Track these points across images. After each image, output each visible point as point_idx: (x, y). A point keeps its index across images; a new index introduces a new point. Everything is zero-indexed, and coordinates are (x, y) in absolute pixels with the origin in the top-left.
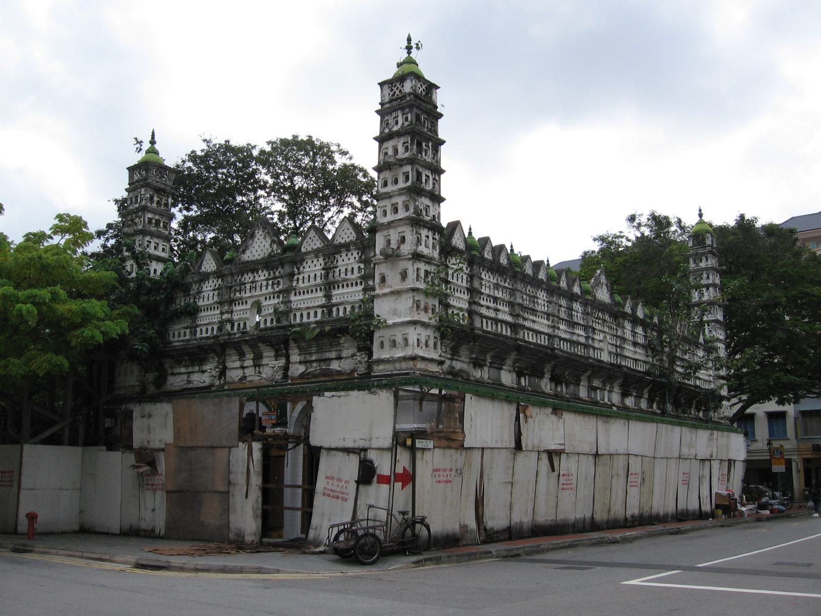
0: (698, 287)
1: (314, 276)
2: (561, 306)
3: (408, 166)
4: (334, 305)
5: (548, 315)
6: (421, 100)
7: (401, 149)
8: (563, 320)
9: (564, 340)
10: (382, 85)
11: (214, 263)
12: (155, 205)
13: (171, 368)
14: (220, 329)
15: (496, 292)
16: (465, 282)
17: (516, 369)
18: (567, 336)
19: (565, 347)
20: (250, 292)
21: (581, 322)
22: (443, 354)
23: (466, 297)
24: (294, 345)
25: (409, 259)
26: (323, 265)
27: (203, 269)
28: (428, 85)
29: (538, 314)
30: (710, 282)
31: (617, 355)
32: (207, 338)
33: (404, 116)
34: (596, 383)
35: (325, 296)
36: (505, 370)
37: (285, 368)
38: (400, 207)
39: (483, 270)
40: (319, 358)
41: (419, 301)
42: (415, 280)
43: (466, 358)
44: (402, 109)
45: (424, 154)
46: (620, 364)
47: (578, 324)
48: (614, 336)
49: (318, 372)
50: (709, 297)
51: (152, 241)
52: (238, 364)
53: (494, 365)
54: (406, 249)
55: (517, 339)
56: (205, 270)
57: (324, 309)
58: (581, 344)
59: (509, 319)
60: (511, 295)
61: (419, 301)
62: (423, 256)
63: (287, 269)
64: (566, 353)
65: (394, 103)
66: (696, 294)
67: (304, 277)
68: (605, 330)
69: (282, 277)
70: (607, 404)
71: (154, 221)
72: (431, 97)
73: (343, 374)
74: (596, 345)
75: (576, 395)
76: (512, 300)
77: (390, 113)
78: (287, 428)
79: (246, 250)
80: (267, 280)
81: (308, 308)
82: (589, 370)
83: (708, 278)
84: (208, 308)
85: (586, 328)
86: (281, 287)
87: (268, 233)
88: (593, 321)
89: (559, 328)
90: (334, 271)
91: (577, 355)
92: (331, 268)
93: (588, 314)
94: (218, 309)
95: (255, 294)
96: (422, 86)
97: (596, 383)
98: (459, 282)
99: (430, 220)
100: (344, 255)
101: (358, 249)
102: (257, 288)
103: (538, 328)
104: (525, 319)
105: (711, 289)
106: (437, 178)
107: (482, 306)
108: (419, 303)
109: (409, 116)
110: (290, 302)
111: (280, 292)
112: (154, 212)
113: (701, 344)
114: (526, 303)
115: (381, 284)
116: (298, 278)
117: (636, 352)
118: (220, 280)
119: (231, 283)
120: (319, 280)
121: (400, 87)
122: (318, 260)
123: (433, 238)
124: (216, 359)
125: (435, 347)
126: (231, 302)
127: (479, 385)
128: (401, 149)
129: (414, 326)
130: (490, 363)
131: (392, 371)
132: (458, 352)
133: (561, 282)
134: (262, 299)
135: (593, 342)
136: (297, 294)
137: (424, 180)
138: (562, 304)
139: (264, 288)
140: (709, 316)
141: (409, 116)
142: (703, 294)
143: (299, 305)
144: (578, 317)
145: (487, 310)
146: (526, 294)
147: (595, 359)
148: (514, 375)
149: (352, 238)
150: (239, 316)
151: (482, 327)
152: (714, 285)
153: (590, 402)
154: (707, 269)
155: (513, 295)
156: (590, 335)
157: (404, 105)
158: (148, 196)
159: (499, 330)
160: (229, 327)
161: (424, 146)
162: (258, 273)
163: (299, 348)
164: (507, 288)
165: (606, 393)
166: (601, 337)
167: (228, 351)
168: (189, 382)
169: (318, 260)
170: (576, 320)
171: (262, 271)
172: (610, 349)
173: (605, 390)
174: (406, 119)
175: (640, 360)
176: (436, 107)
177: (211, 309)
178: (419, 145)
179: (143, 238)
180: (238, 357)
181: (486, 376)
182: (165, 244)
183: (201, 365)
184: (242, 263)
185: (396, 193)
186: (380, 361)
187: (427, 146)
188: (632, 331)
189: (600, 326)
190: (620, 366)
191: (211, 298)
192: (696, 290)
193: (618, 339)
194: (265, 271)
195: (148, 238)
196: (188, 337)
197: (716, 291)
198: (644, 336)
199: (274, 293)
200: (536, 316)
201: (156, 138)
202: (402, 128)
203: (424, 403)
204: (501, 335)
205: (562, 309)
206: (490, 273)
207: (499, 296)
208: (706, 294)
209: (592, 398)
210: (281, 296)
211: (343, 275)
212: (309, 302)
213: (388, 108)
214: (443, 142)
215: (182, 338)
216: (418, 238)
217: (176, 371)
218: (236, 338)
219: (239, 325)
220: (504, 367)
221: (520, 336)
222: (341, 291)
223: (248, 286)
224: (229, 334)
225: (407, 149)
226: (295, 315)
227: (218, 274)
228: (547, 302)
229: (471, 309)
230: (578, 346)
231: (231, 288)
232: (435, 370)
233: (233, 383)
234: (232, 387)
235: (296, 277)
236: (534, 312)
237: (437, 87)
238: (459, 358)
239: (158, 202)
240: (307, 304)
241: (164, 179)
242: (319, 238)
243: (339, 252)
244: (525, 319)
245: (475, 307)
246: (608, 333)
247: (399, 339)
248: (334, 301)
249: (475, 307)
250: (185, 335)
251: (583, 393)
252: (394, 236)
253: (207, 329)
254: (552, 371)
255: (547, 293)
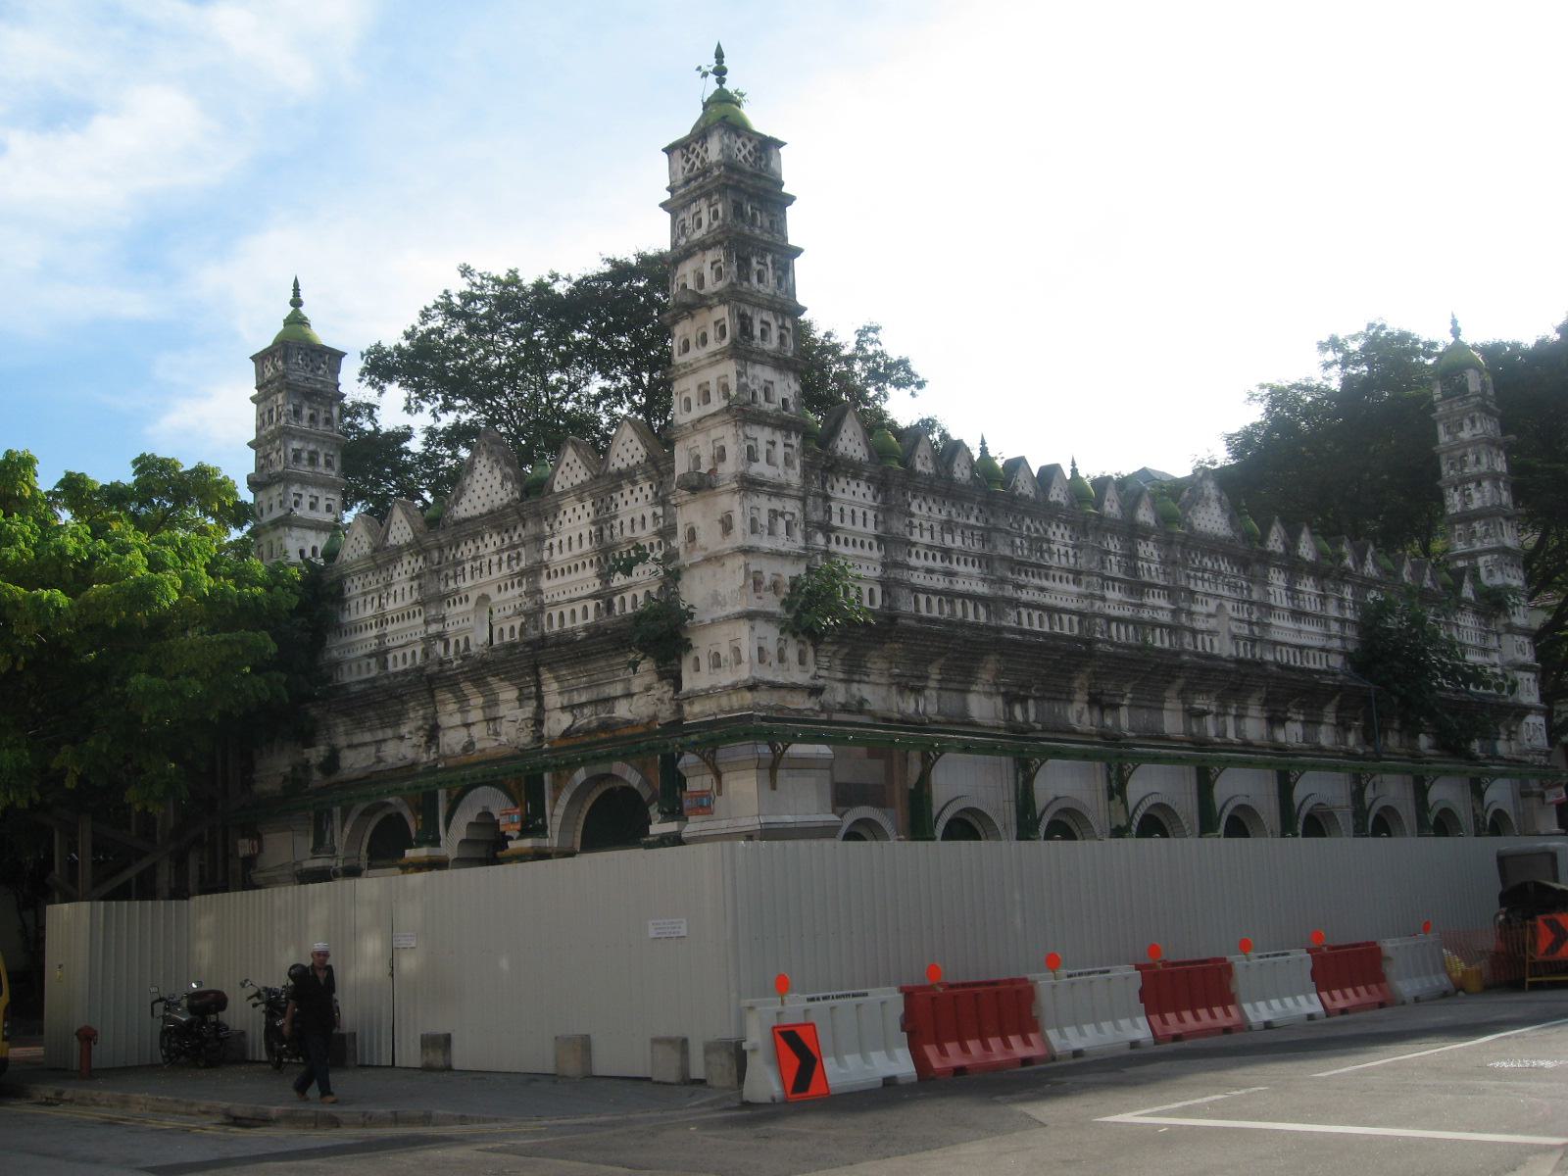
0: (1461, 483)
2: (1108, 552)
5: (1077, 575)
8: (1114, 579)
9: (1119, 620)
10: (669, 150)
12: (305, 424)
13: (347, 734)
15: (948, 538)
17: (1002, 690)
20: (472, 577)
21: (1161, 581)
23: (876, 554)
24: (548, 675)
26: (592, 515)
27: (392, 541)
30: (1483, 468)
34: (1200, 703)
36: (978, 692)
40: (594, 697)
42: (748, 531)
44: (708, 195)
47: (1154, 586)
48: (1244, 602)
49: (595, 724)
50: (1484, 502)
51: (303, 492)
52: (457, 719)
54: (729, 468)
55: (999, 630)
57: (599, 601)
58: (1162, 626)
59: (981, 589)
62: (762, 484)
63: (531, 528)
64: (1123, 648)
65: (693, 184)
66: (1457, 496)
68: (1220, 592)
69: (523, 544)
70: (1231, 744)
71: (305, 455)
72: (767, 165)
76: (986, 550)
77: (685, 207)
78: (546, 837)
79: (460, 498)
80: (499, 551)
81: (572, 601)
83: (1478, 461)
85: (1171, 592)
87: (497, 461)
89: (1103, 599)
90: (612, 526)
92: (606, 521)
93: (1174, 563)
94: (420, 614)
95: (481, 581)
96: (744, 145)
97: (1200, 703)
99: (776, 410)
101: (649, 478)
104: (1019, 587)
105: (1486, 484)
107: (916, 569)
108: (759, 577)
109: (720, 207)
110: (540, 592)
111: (522, 573)
112: (304, 436)
113: (1467, 601)
114: (1023, 553)
115: (689, 545)
116: (551, 544)
117: (1300, 631)
120: (586, 546)
122: (583, 507)
125: (802, 662)
126: (442, 598)
131: (715, 714)
132: (860, 666)
133: (1106, 503)
134: (492, 591)
137: (757, 332)
139: (495, 568)
140: (1486, 541)
141: (720, 207)
142: (1469, 495)
143: (556, 596)
145: (928, 576)
146: (1021, 536)
148: (999, 701)
150: (456, 627)
152: (1495, 477)
154: (1474, 442)
155: (989, 541)
156: (1184, 605)
157: (710, 187)
158: (291, 407)
159: (959, 614)
160: (439, 647)
162: (482, 539)
164: (973, 527)
165: (1230, 722)
167: (440, 696)
168: (380, 760)
169: (583, 507)
172: (1235, 630)
173: (1226, 714)
174: (716, 215)
175: (1310, 648)
178: (744, 264)
179: (286, 488)
180: (457, 706)
182: (331, 496)
183: (397, 724)
185: (703, 362)
186: (694, 696)
188: (1287, 589)
189: (1207, 584)
192: (1456, 490)
193: (1255, 608)
194: (495, 536)
195: (295, 489)
196: (373, 674)
197: (1497, 487)
198: (1319, 596)
200: (1047, 579)
201: (301, 293)
202: (708, 233)
203: (780, 773)
205: (1112, 557)
208: (1476, 495)
209: (1192, 735)
210: (524, 581)
211: (627, 533)
212: (573, 590)
213: (683, 196)
214: (797, 252)
215: (365, 676)
216: (749, 448)
217: (356, 740)
219: (457, 642)
220: (974, 688)
223: (468, 567)
224: (441, 663)
225: (719, 274)
226: (550, 616)
232: (802, 707)
233: (454, 756)
234: (451, 762)
235: (547, 543)
237: (782, 144)
238: (866, 678)
239: (312, 418)
240: (572, 595)
241: (320, 372)
244: (1019, 587)
246: (1228, 599)
247: (725, 652)
250: (369, 670)
251: (1172, 722)
255: (1073, 529)
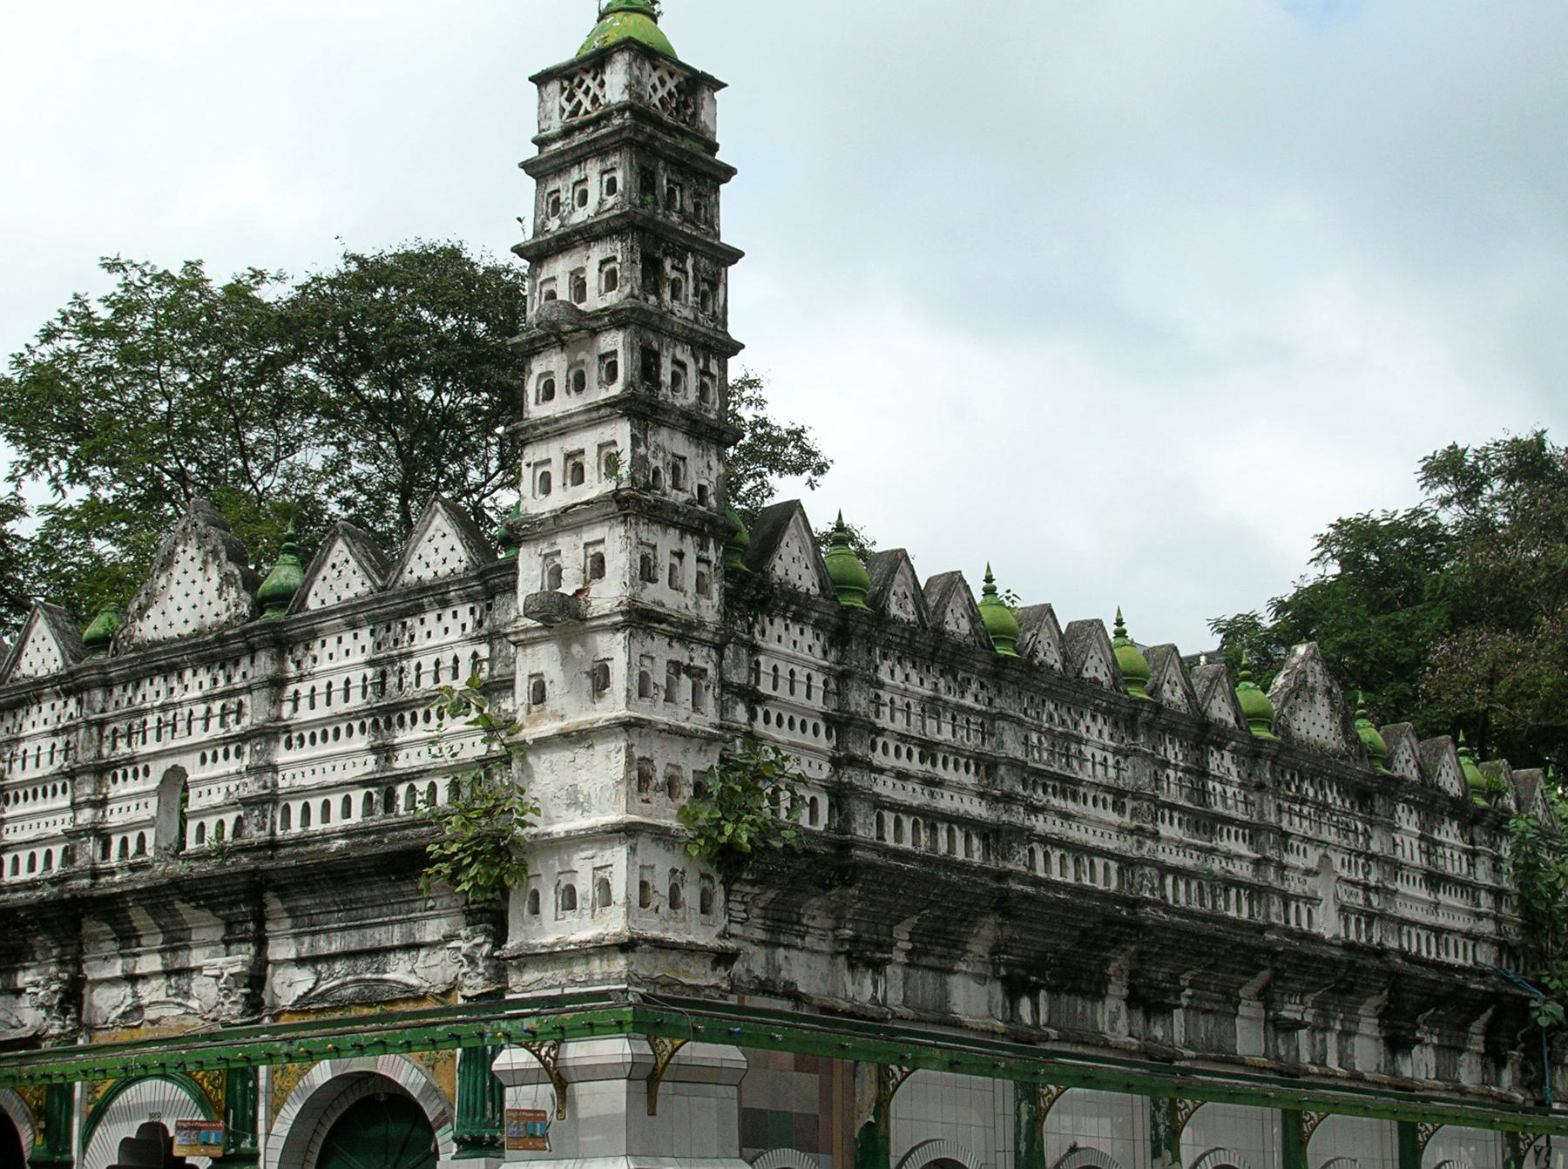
1: (450, 663)
2: (1165, 764)
3: (613, 333)
4: (399, 779)
5: (1118, 797)
6: (657, 122)
7: (593, 278)
8: (1173, 807)
9: (1178, 872)
11: (56, 651)
14: (68, 857)
15: (931, 724)
16: (818, 694)
17: (1003, 972)
18: (1188, 861)
19: (1179, 894)
20: (159, 739)
21: (1238, 813)
22: (736, 929)
23: (823, 743)
25: (615, 628)
28: (687, 80)
29: (1082, 790)
31: (1371, 917)
32: (31, 885)
33: (606, 177)
35: (373, 750)
37: (251, 977)
38: (590, 461)
39: (885, 656)
41: (650, 761)
42: (635, 695)
43: (823, 938)
45: (667, 296)
46: (1380, 944)
47: (1230, 821)
53: (924, 961)
54: (607, 596)
56: (30, 672)
57: (371, 790)
58: (1239, 884)
59: (977, 809)
60: (985, 734)
61: (650, 761)
62: (661, 619)
63: (264, 666)
64: (1181, 916)
65: (578, 138)
67: (313, 689)
68: (1325, 836)
69: (249, 690)
72: (695, 115)
73: (421, 998)
74: (1294, 886)
75: (1220, 1050)
76: (987, 748)
77: (560, 171)
79: (147, 607)
80: (206, 699)
82: (1263, 968)
84: (35, 792)
85: (1254, 831)
86: (246, 721)
87: (215, 553)
88: (1280, 809)
89: (1156, 836)
90: (402, 670)
91: (1223, 920)
92: (391, 660)
93: (1260, 787)
94: (64, 792)
96: (663, 83)
98: (800, 697)
99: (688, 502)
100: (430, 617)
101: (470, 598)
102: (179, 726)
103: (1087, 837)
106: (714, 369)
107: (881, 771)
108: (647, 767)
111: (243, 738)
114: (1039, 759)
115: (534, 708)
116: (296, 692)
117: (1437, 905)
118: (72, 702)
119: (103, 711)
121: (595, 89)
122: (356, 636)
123: (699, 560)
124: (55, 952)
125: (705, 909)
126: (103, 770)
127: (859, 1028)
128: (593, 278)
129: (631, 842)
130: (909, 953)
134: (190, 763)
135: (1283, 878)
136: (295, 742)
137: (666, 377)
138: (1171, 755)
139: (198, 726)
143: (299, 776)
144: (1227, 798)
145: (899, 783)
146: (1038, 729)
147: (1289, 933)
148: (997, 989)
149: (456, 565)
151: (881, 837)
153: (1272, 1069)
156: (1271, 853)
161: (668, 268)
162: (180, 676)
163: (292, 913)
164: (970, 711)
165: (1331, 1039)
166: (1312, 859)
169: (356, 636)
170: (1219, 809)
171: (195, 674)
174: (612, 185)
176: (713, 147)
177: (45, 795)
181: (895, 997)
184: (137, 648)
186: (527, 959)
187: (683, 272)
188: (1421, 838)
190: (1381, 952)
191: (45, 759)
198: (1465, 851)
199: (226, 741)
200: (1074, 800)
203: (663, 1088)
204: (948, 863)
205: (1171, 772)
206: (909, 665)
207: (940, 738)
209: (1278, 1058)
210: (247, 749)
211: (427, 682)
214: (734, 255)
216: (644, 558)
218: (114, 885)
219: (124, 841)
221: (1017, 864)
222: (420, 732)
223: (152, 721)
224: (95, 874)
225: (611, 281)
226: (287, 809)
227: (68, 685)
228: (1116, 752)
229: (840, 783)
230: (1227, 890)
231: (101, 724)
235: (291, 689)
236: (1068, 786)
242: (360, 563)
243: (419, 610)
244: (1034, 809)
245: (851, 775)
246: (1337, 848)
248: (402, 763)
249: (851, 775)
251: (1248, 1039)
252: (571, 552)
253: (32, 856)
254: (1133, 974)
255: (1116, 724)
